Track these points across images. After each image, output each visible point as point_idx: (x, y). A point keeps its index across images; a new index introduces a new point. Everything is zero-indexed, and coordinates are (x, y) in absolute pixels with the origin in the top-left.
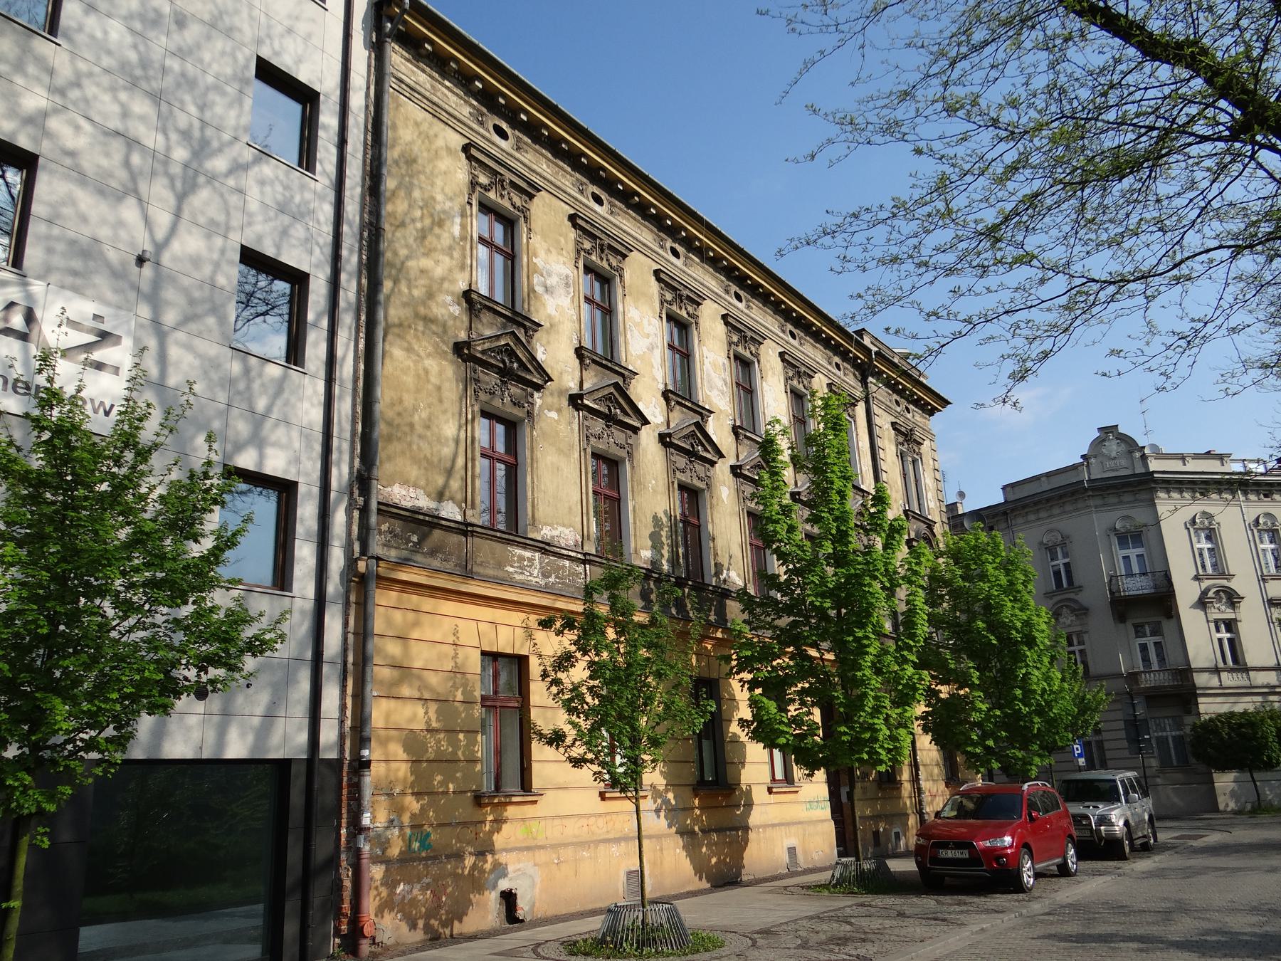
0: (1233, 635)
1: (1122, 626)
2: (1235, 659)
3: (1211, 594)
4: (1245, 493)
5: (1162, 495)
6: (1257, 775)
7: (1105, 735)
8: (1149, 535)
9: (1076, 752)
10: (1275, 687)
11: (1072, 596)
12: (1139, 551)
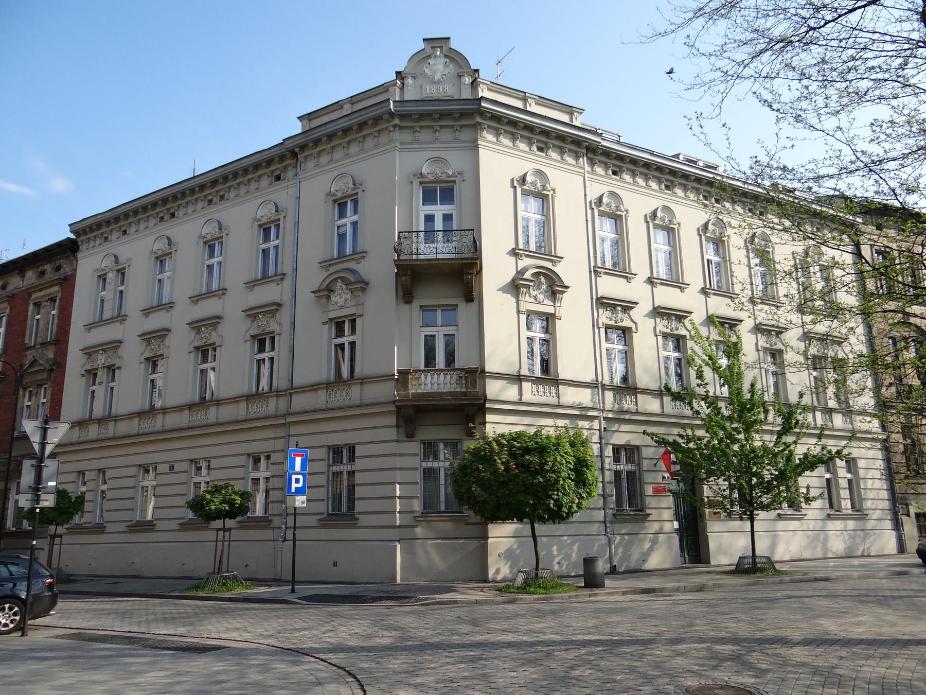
2: (546, 366)
3: (527, 275)
4: (592, 163)
5: (489, 136)
6: (540, 528)
7: (359, 464)
8: (461, 191)
9: (294, 485)
11: (351, 265)
12: (447, 209)
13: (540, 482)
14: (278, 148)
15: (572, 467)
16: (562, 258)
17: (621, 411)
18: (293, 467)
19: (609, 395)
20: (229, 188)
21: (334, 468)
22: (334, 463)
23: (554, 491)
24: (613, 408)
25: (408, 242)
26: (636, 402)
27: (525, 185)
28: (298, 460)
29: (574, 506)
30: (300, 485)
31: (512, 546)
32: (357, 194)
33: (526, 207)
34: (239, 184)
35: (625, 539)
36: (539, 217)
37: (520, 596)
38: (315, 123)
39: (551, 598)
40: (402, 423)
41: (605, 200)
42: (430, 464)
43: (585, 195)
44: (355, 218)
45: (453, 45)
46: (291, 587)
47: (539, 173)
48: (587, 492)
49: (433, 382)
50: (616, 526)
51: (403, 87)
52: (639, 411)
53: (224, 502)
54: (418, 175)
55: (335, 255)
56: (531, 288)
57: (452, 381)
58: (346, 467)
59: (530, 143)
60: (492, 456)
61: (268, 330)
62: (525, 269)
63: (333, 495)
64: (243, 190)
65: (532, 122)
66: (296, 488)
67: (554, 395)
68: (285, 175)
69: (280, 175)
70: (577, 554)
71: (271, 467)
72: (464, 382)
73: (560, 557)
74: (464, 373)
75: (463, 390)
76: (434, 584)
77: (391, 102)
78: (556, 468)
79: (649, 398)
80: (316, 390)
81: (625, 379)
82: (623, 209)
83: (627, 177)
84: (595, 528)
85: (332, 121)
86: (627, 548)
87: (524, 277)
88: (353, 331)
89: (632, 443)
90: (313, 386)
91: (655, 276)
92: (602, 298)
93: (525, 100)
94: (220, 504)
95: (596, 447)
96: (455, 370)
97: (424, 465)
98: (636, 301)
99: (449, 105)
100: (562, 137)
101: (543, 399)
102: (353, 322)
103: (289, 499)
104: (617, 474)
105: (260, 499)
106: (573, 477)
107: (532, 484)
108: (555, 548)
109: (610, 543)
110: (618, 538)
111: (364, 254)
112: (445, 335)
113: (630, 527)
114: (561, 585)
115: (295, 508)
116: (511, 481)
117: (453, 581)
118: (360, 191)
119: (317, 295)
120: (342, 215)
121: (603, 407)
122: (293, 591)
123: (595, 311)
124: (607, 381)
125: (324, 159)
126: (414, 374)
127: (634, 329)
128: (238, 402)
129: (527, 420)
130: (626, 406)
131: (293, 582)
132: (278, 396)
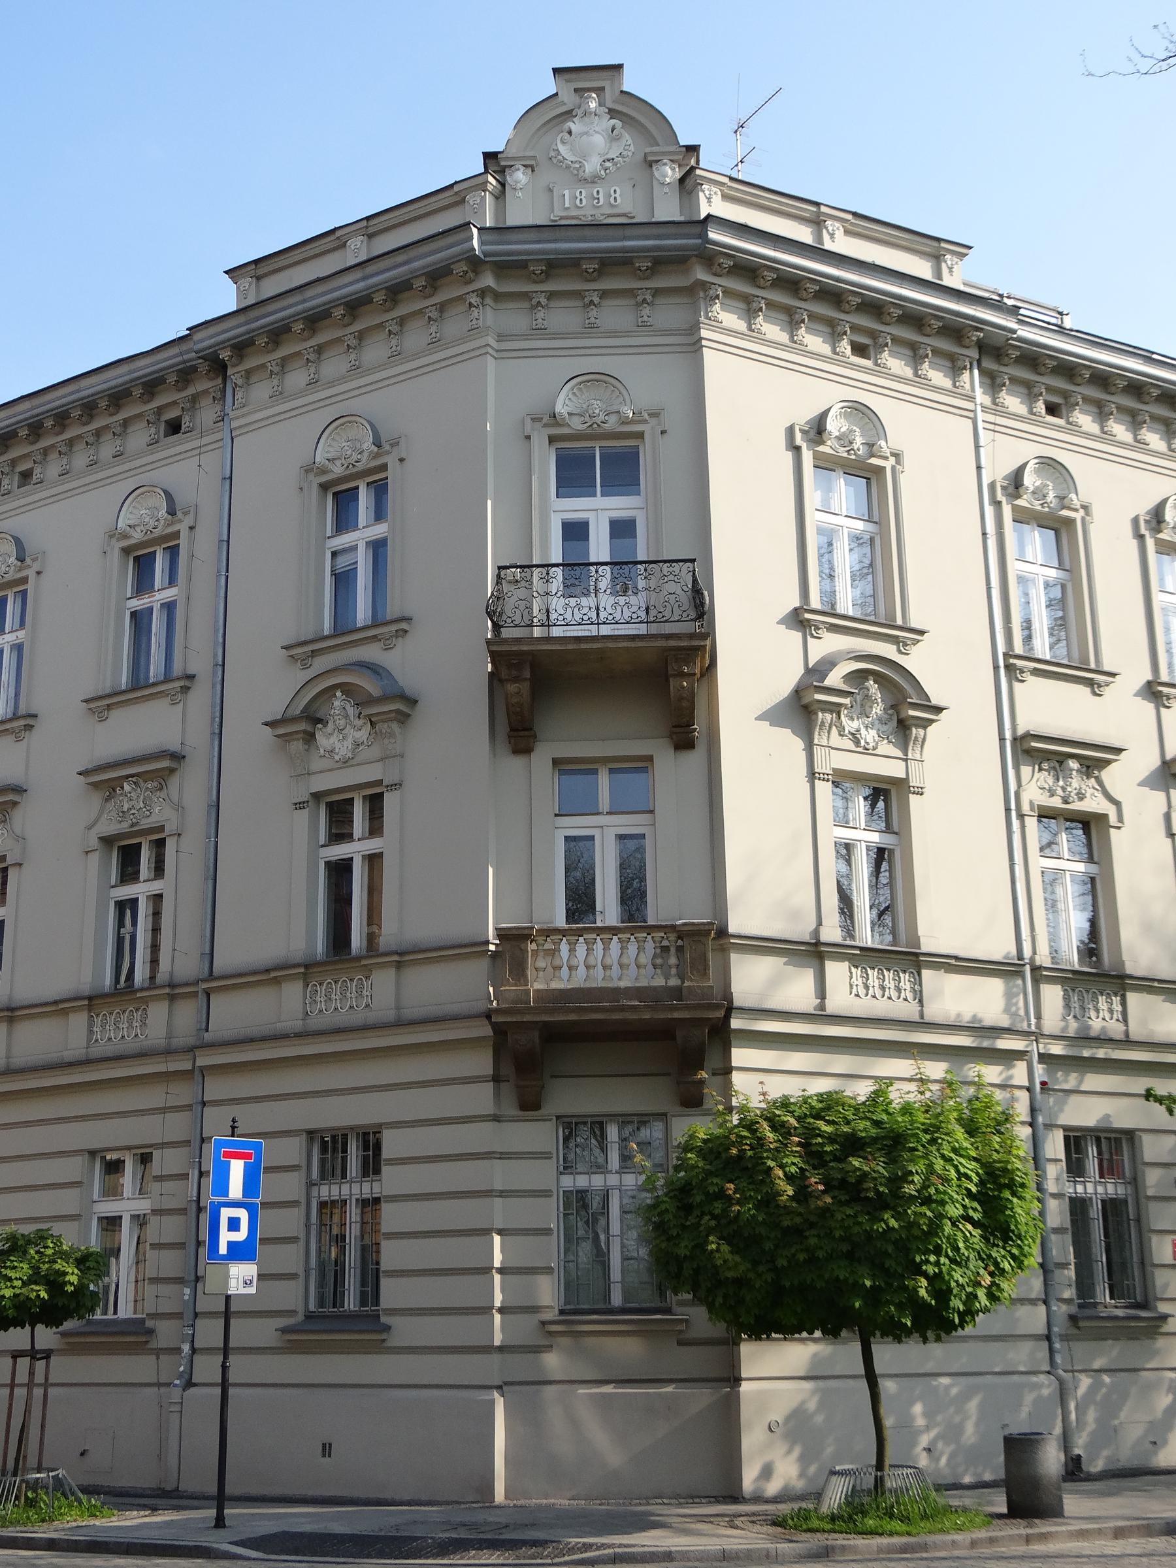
0: (887, 840)
1: (517, 763)
3: (834, 679)
4: (993, 383)
5: (730, 319)
6: (886, 1354)
7: (392, 1180)
9: (226, 1237)
10: (996, 1031)
11: (371, 653)
12: (620, 505)
13: (891, 1229)
14: (174, 351)
15: (974, 1189)
16: (922, 633)
17: (1085, 1038)
18: (223, 1186)
19: (1052, 995)
20: (45, 452)
21: (324, 1190)
22: (323, 1176)
23: (927, 1252)
24: (1065, 1029)
25: (522, 593)
26: (1124, 1013)
27: (822, 442)
28: (237, 1169)
29: (981, 1294)
30: (241, 1235)
31: (803, 1402)
32: (384, 467)
33: (826, 500)
34: (71, 443)
35: (1102, 1384)
36: (860, 525)
37: (839, 1540)
38: (272, 287)
39: (925, 1547)
40: (508, 1070)
41: (1030, 480)
42: (582, 1181)
43: (979, 468)
44: (380, 530)
45: (630, 83)
46: (213, 1512)
47: (859, 411)
48: (1013, 1257)
49: (591, 961)
50: (1079, 1348)
51: (503, 192)
52: (1133, 1037)
53: (35, 1278)
54: (546, 420)
55: (327, 627)
56: (843, 712)
57: (643, 960)
58: (356, 1189)
59: (834, 333)
60: (758, 1160)
61: (146, 823)
62: (828, 664)
63: (322, 1266)
64: (80, 459)
65: (838, 279)
66: (231, 1245)
67: (910, 996)
68: (192, 416)
69: (179, 418)
70: (977, 1424)
71: (155, 1187)
72: (673, 960)
73: (933, 1434)
74: (672, 937)
75: (674, 982)
76: (595, 1506)
77: (475, 231)
78: (932, 1191)
79: (1156, 1000)
80: (277, 981)
81: (1091, 949)
82: (1076, 503)
83: (1085, 420)
84: (1023, 1355)
85: (319, 280)
86: (1109, 1409)
87: (828, 682)
88: (375, 827)
89: (1118, 1124)
90: (268, 971)
91: (1164, 677)
92: (1029, 736)
93: (817, 223)
94: (24, 1284)
95: (1025, 1132)
96: (651, 929)
97: (567, 1182)
98: (1117, 744)
99: (625, 238)
100: (915, 318)
101: (881, 1007)
102: (375, 803)
103: (211, 1273)
104: (1078, 1206)
105: (123, 1271)
106: (976, 1216)
107: (869, 1236)
108: (918, 1409)
109: (1063, 1394)
110: (1085, 1382)
111: (404, 626)
112: (621, 838)
113: (1115, 1353)
114: (948, 1510)
115: (228, 1297)
116: (812, 1225)
117: (647, 1499)
118: (391, 460)
119: (281, 731)
120: (344, 521)
121: (1038, 1026)
122: (220, 1522)
123: (1011, 772)
124: (1044, 959)
125: (297, 378)
126: (540, 939)
127: (1113, 820)
128: (65, 1012)
129: (842, 1063)
130: (1096, 1024)
131: (221, 1499)
132: (172, 998)
